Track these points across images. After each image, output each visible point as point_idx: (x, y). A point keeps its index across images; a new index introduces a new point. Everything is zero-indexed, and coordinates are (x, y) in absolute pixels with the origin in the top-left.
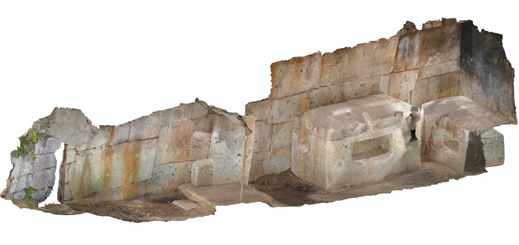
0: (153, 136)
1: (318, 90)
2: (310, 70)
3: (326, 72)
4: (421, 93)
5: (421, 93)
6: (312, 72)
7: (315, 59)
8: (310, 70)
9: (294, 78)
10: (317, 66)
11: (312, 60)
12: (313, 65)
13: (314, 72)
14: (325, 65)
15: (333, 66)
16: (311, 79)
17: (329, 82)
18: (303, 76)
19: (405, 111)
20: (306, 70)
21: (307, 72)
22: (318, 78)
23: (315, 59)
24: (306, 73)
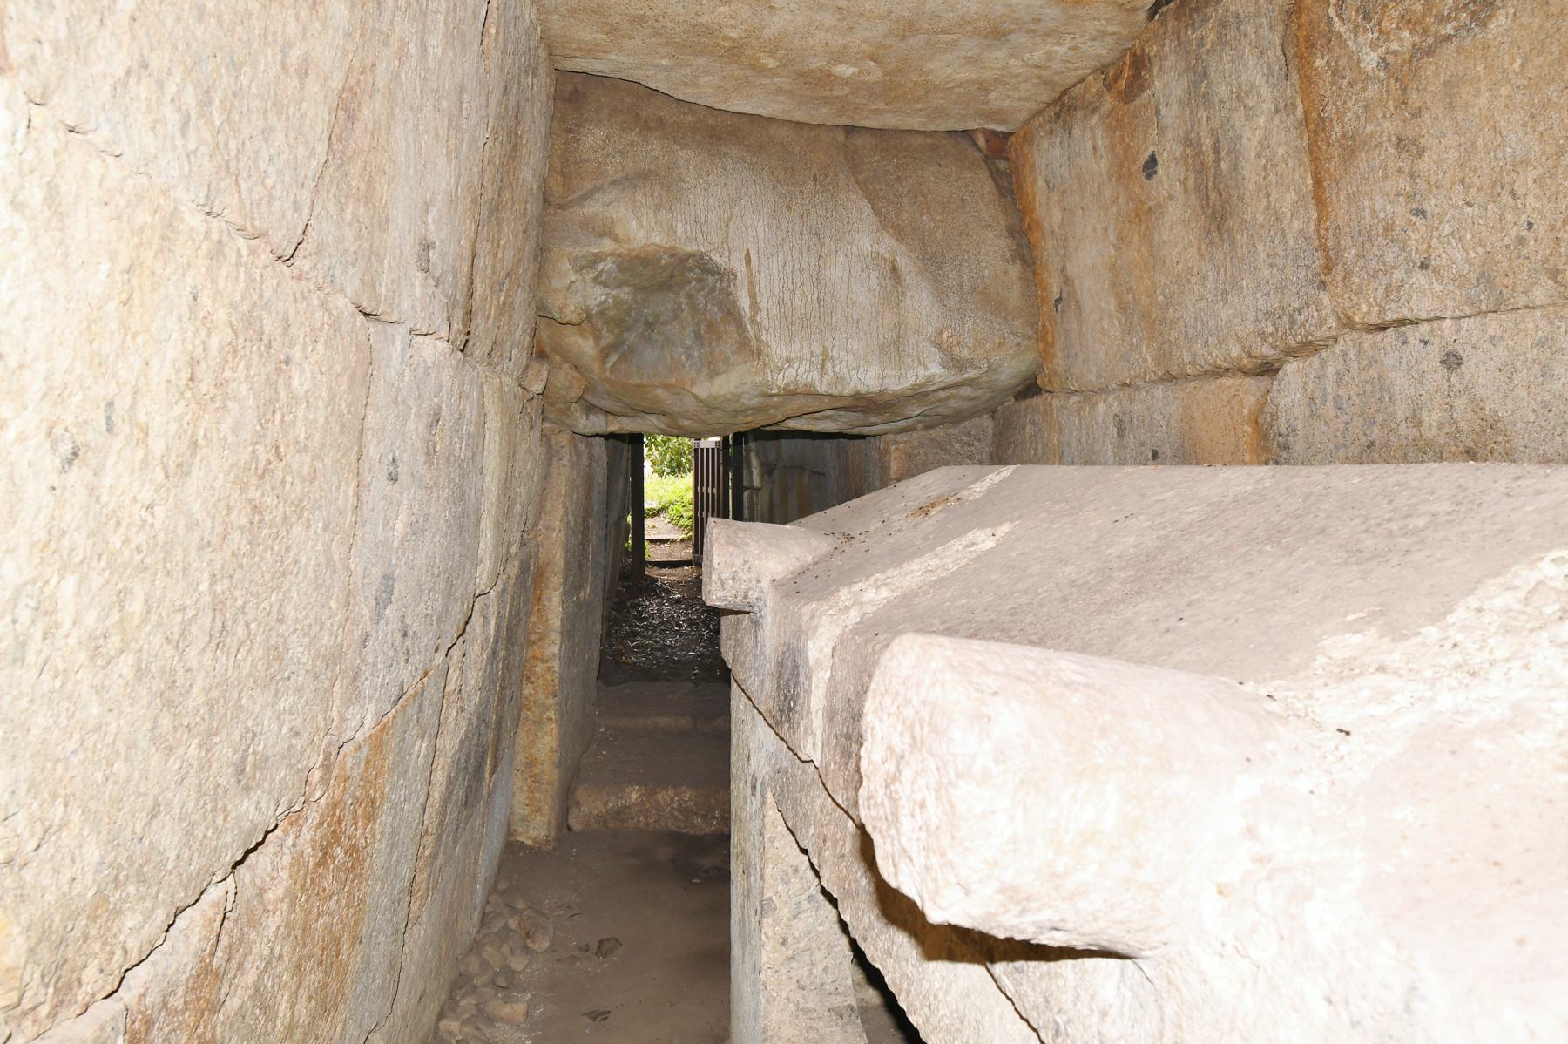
0: (1207, 387)
1: (1324, 363)
2: (1216, 151)
3: (1352, 147)
4: (40, 584)
5: (40, 584)
6: (1235, 167)
7: (1223, 24)
8: (1216, 151)
9: (1121, 238)
10: (1265, 92)
11: (1201, 44)
12: (1223, 90)
13: (1250, 172)
14: (1319, 63)
15: (1429, 52)
16: (1241, 239)
17: (1424, 266)
18: (1174, 213)
19: (499, 817)
20: (1185, 158)
21: (1201, 170)
22: (1300, 223)
23: (1223, 24)
24: (1191, 181)
